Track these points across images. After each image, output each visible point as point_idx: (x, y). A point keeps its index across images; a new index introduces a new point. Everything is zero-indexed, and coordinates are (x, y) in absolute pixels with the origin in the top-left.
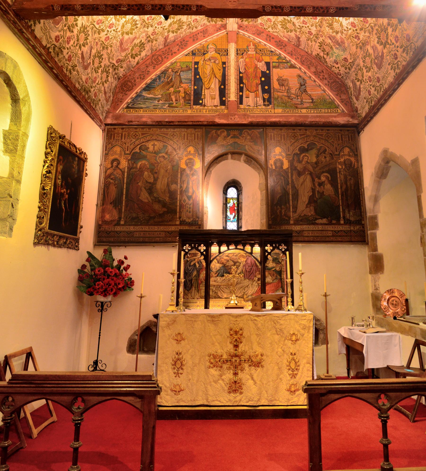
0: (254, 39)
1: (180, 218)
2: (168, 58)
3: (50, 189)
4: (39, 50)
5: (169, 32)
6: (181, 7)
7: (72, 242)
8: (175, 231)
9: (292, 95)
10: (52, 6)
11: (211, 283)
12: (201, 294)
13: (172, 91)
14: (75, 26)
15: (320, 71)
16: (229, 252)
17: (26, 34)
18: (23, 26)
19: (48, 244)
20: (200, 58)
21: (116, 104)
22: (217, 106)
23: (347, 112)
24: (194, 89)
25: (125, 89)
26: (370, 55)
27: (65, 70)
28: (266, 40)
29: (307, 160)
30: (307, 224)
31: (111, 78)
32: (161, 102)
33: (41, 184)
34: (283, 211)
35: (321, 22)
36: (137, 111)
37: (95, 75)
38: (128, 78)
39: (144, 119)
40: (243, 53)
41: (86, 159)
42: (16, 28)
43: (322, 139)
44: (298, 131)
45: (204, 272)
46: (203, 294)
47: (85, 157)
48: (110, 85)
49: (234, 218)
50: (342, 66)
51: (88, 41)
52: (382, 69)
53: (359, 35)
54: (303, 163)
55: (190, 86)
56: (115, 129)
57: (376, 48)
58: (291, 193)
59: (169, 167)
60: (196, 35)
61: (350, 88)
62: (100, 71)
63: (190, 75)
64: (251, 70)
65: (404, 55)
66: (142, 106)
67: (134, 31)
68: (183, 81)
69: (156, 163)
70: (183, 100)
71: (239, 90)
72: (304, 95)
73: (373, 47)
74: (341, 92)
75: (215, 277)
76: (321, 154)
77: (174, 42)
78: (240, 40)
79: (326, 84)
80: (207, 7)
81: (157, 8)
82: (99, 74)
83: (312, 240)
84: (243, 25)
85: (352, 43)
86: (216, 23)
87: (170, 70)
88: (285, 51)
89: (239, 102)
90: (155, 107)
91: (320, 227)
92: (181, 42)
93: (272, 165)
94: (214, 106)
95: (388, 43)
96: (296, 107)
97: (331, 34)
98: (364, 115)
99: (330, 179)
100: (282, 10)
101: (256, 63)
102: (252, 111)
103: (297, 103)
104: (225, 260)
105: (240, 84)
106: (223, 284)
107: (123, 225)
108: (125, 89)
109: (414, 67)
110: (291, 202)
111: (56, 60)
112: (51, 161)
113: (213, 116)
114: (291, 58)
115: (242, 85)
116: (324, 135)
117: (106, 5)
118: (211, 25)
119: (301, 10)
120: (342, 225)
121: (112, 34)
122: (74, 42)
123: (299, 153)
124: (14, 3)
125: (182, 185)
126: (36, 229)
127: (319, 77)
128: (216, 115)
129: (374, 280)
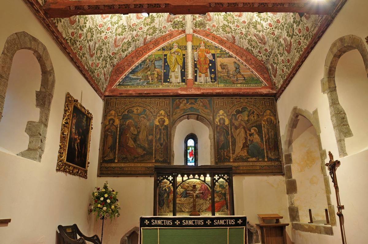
0: (204, 39)
1: (155, 158)
2: (146, 52)
3: (68, 134)
4: (60, 40)
5: (147, 35)
6: (154, 5)
7: (82, 173)
8: (152, 167)
9: (230, 75)
10: (69, 7)
11: (177, 202)
12: (170, 209)
13: (149, 74)
14: (85, 27)
15: (249, 59)
16: (189, 180)
17: (52, 28)
18: (50, 22)
19: (66, 172)
20: (168, 52)
21: (111, 83)
22: (180, 83)
23: (268, 86)
24: (164, 72)
25: (118, 73)
26: (282, 45)
27: (78, 56)
28: (212, 40)
29: (241, 118)
30: (242, 162)
31: (109, 65)
32: (141, 81)
33: (61, 130)
34: (225, 153)
35: (249, 25)
36: (125, 87)
37: (97, 61)
38: (120, 66)
39: (130, 92)
40: (197, 48)
41: (92, 117)
42: (45, 23)
43: (252, 104)
44: (235, 99)
45: (172, 195)
46: (172, 209)
47: (91, 116)
48: (108, 70)
49: (192, 160)
50: (264, 55)
51: (93, 38)
52: (290, 54)
53: (274, 32)
54: (239, 120)
55: (161, 70)
56: (111, 99)
57: (286, 39)
58: (230, 141)
59: (147, 124)
60: (165, 37)
61: (270, 70)
62: (101, 59)
63: (161, 63)
64: (202, 59)
65: (305, 41)
66: (129, 84)
67: (123, 34)
68: (157, 67)
69: (138, 121)
70: (156, 79)
71: (194, 72)
72: (238, 75)
73: (284, 39)
74: (264, 72)
75: (180, 198)
76: (250, 115)
77: (150, 42)
78: (194, 40)
79: (253, 68)
80: (172, 4)
81: (138, 7)
82: (101, 61)
83: (246, 172)
84: (197, 30)
85: (270, 38)
86: (178, 29)
87: (148, 60)
88: (225, 46)
89: (194, 80)
90: (138, 85)
91: (251, 164)
92: (155, 42)
93: (217, 122)
94: (178, 83)
95: (294, 35)
96: (234, 83)
97: (255, 33)
98: (280, 87)
99: (257, 131)
100: (223, 5)
101: (206, 54)
102: (203, 86)
103: (234, 80)
104: (187, 186)
105: (195, 69)
106: (185, 202)
107: (117, 163)
108: (118, 73)
109: (312, 48)
110: (231, 146)
111: (72, 48)
112: (68, 116)
113: (177, 89)
114: (229, 51)
115: (196, 69)
116: (253, 102)
117: (104, 5)
118: (175, 30)
119: (235, 6)
120: (266, 161)
121: (109, 35)
122: (84, 38)
123: (236, 114)
124: (44, 5)
125: (156, 136)
126: (58, 160)
127: (248, 63)
128: (179, 89)
129: (291, 198)
